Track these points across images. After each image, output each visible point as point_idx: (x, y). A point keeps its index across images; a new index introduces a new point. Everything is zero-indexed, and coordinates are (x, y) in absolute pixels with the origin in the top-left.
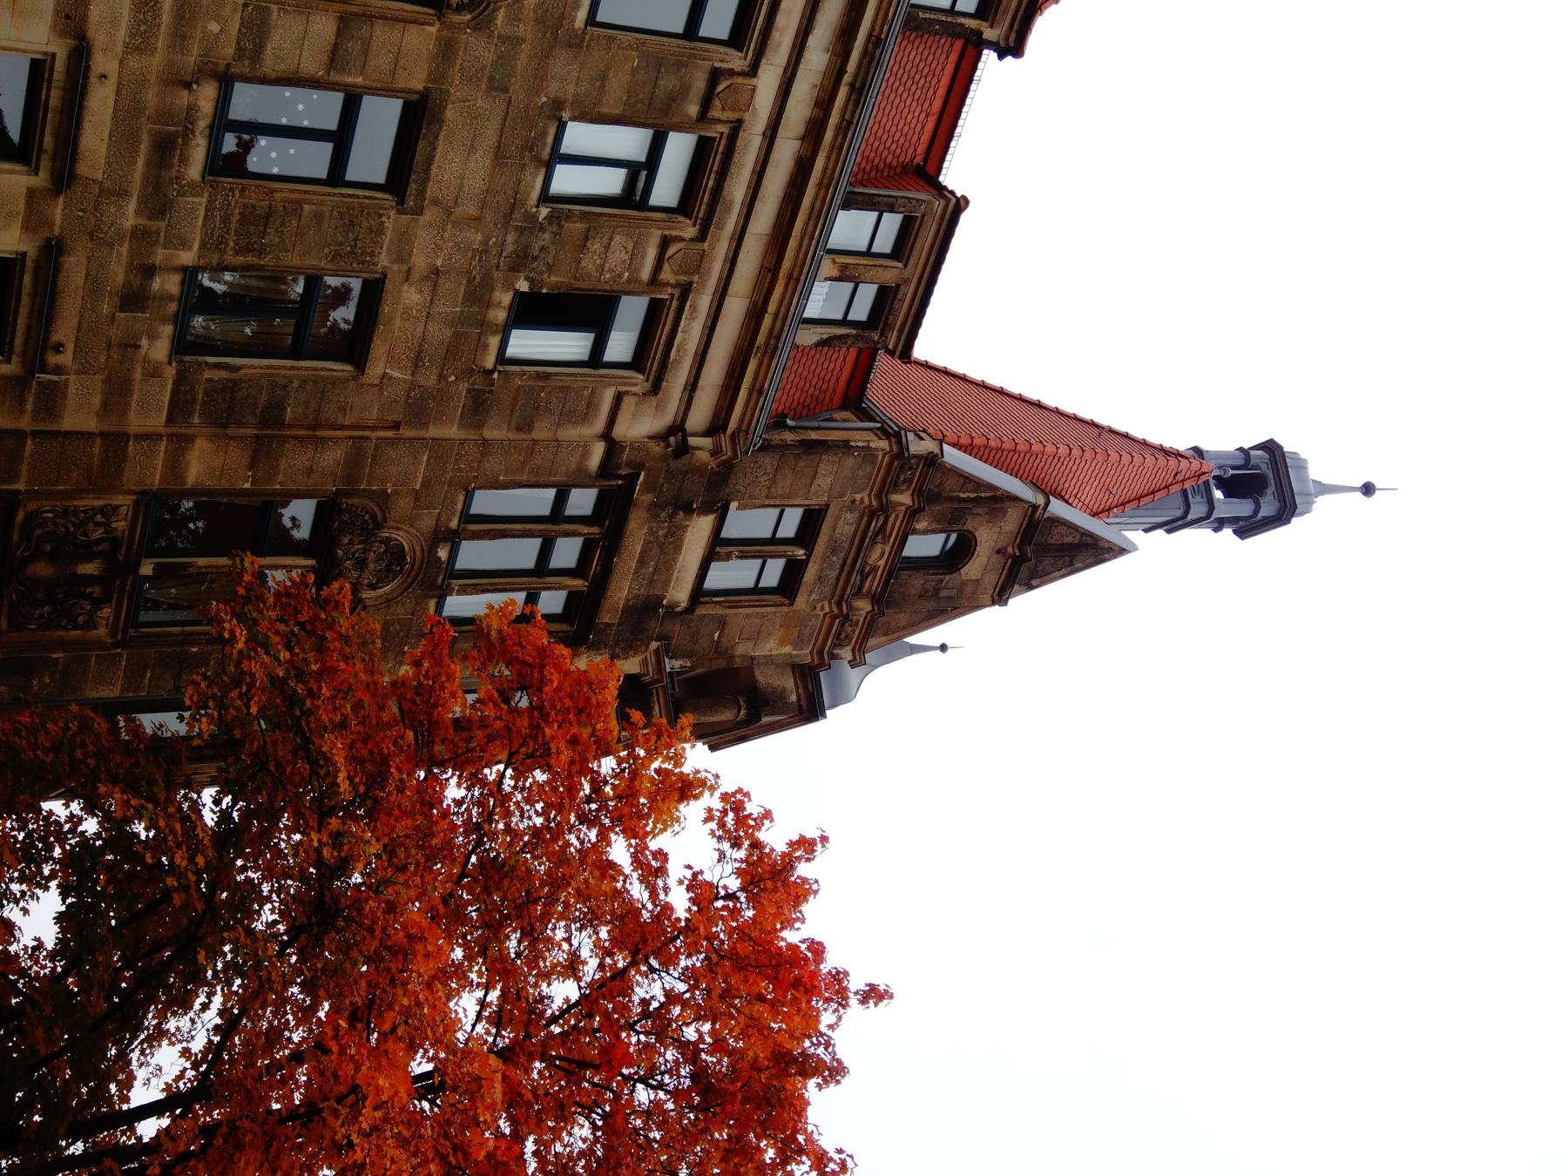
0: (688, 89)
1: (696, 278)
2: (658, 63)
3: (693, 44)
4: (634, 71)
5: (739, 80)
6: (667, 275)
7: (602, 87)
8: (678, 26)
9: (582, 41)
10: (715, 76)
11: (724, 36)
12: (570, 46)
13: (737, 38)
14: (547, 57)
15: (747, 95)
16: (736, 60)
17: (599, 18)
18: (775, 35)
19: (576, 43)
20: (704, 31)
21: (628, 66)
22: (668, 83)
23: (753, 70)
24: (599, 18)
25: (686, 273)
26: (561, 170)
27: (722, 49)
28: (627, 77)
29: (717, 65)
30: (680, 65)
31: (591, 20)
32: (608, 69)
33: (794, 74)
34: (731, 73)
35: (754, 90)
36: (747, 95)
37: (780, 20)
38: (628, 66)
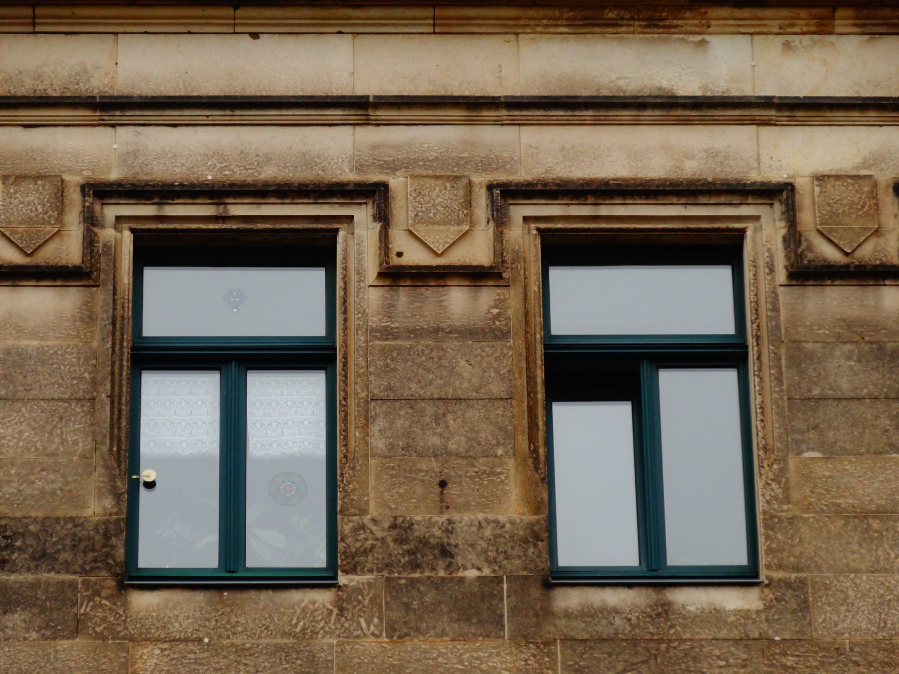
0: (849, 324)
1: (480, 179)
2: (805, 403)
3: (751, 341)
4: (831, 453)
5: (807, 218)
6: (478, 251)
7: (881, 513)
8: (726, 380)
9: (788, 584)
10: (807, 273)
11: (723, 274)
12: (805, 607)
13: (719, 248)
14: (839, 651)
15: (836, 190)
16: (765, 235)
17: (741, 559)
18: (692, 168)
19: (796, 597)
20: (722, 324)
21: (822, 470)
22: (843, 372)
23: (778, 193)
24: (741, 559)
25: (468, 203)
26: (679, 553)
27: (748, 275)
28: (849, 465)
29: (781, 276)
30: (799, 357)
31: (743, 577)
32: (839, 511)
33: (767, 103)
34: (793, 237)
35: (820, 179)
36: (836, 190)
37: (656, 168)
38: (822, 470)
